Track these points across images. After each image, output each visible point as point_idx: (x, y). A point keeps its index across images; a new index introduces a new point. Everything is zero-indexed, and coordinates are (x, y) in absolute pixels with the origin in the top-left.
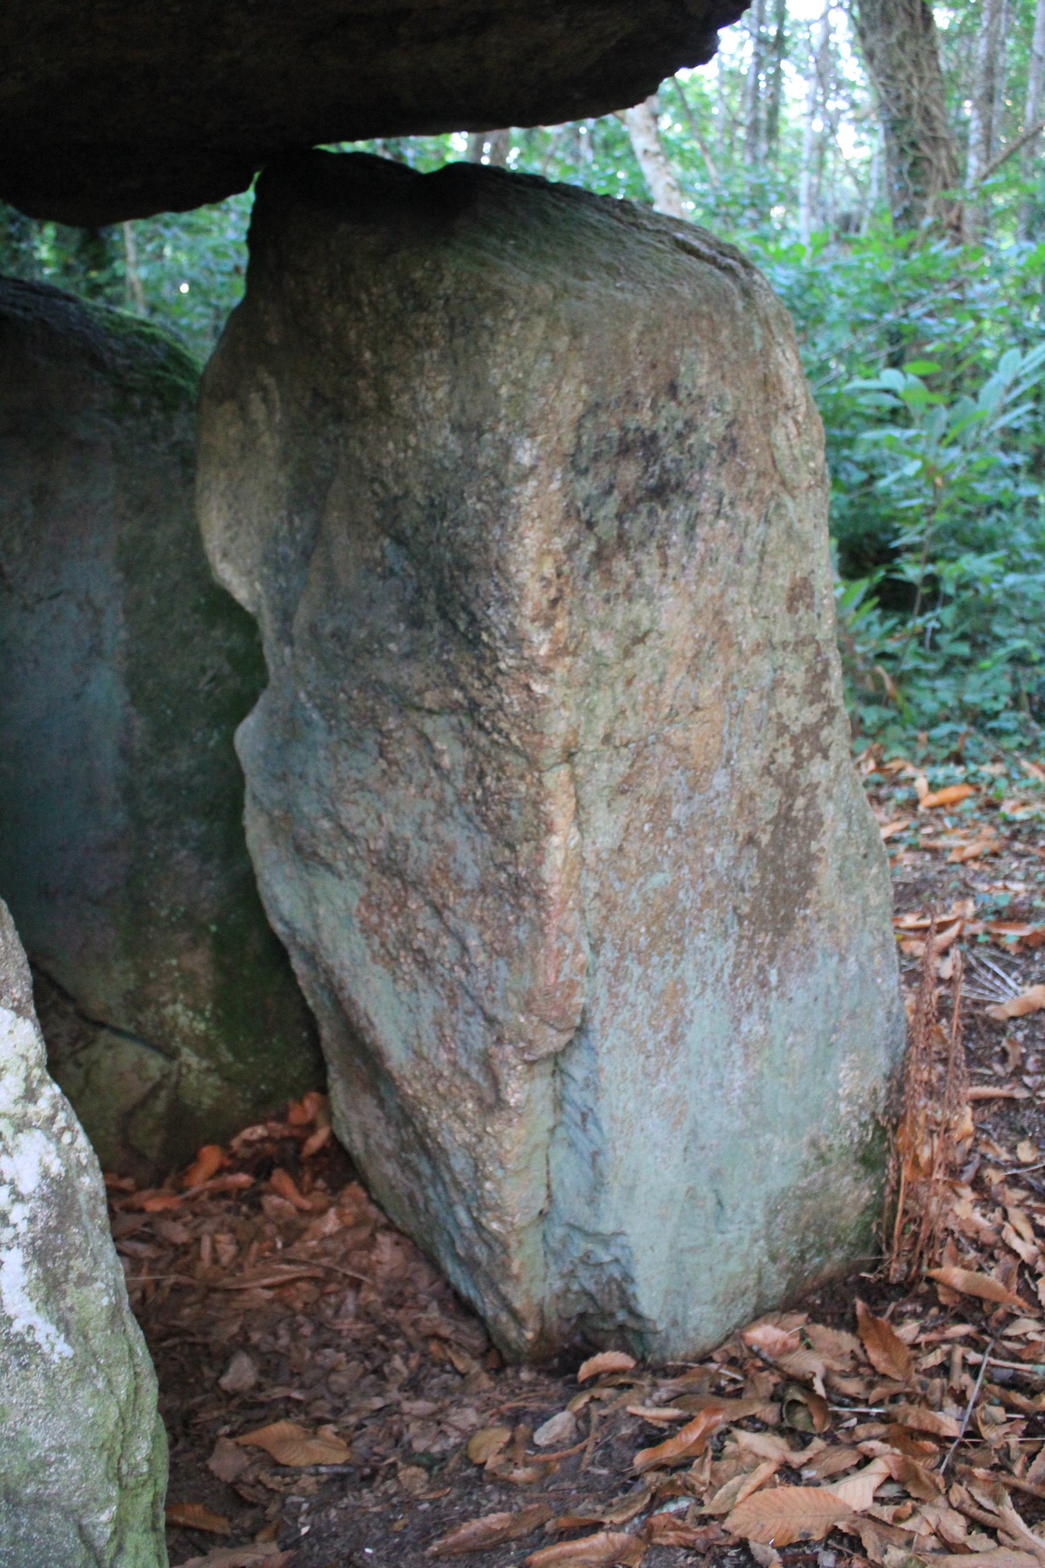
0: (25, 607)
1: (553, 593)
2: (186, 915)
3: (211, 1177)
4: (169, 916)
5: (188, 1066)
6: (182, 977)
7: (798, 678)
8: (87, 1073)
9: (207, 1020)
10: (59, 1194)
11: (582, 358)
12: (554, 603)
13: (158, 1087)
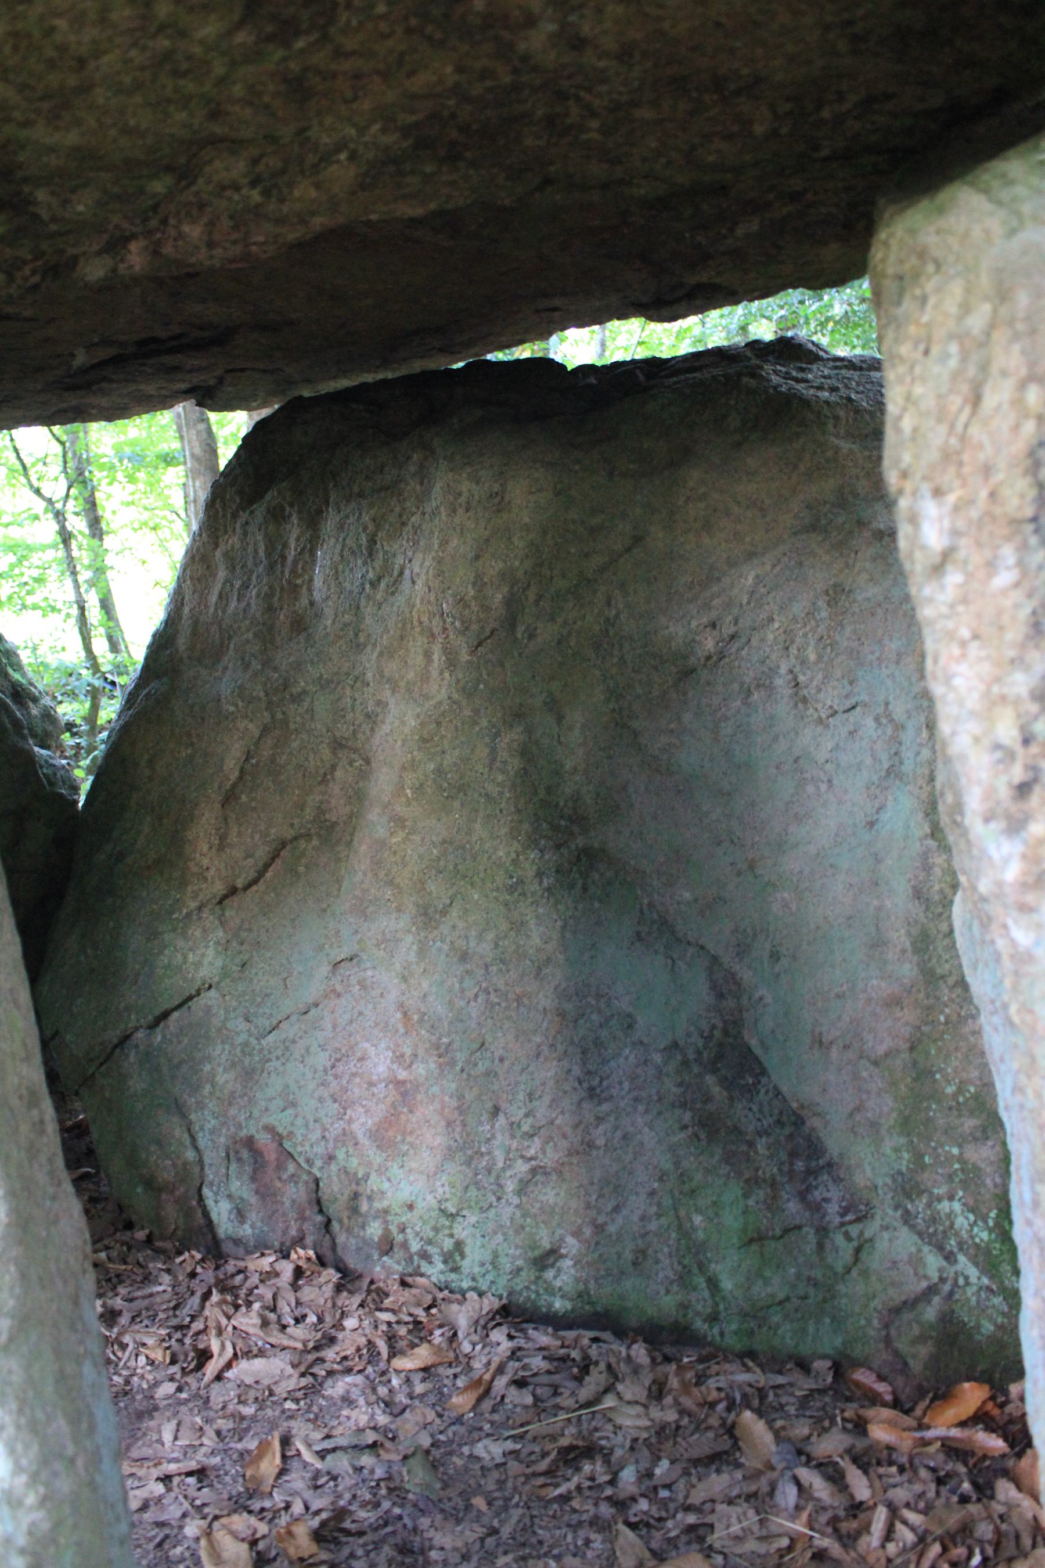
0: (820, 721)
1: (1018, 773)
2: (976, 1097)
3: (962, 1424)
4: (955, 1096)
5: (967, 1278)
6: (962, 1170)
8: (858, 1250)
9: (990, 1230)
11: (1016, 337)
12: (1023, 790)
13: (932, 1290)
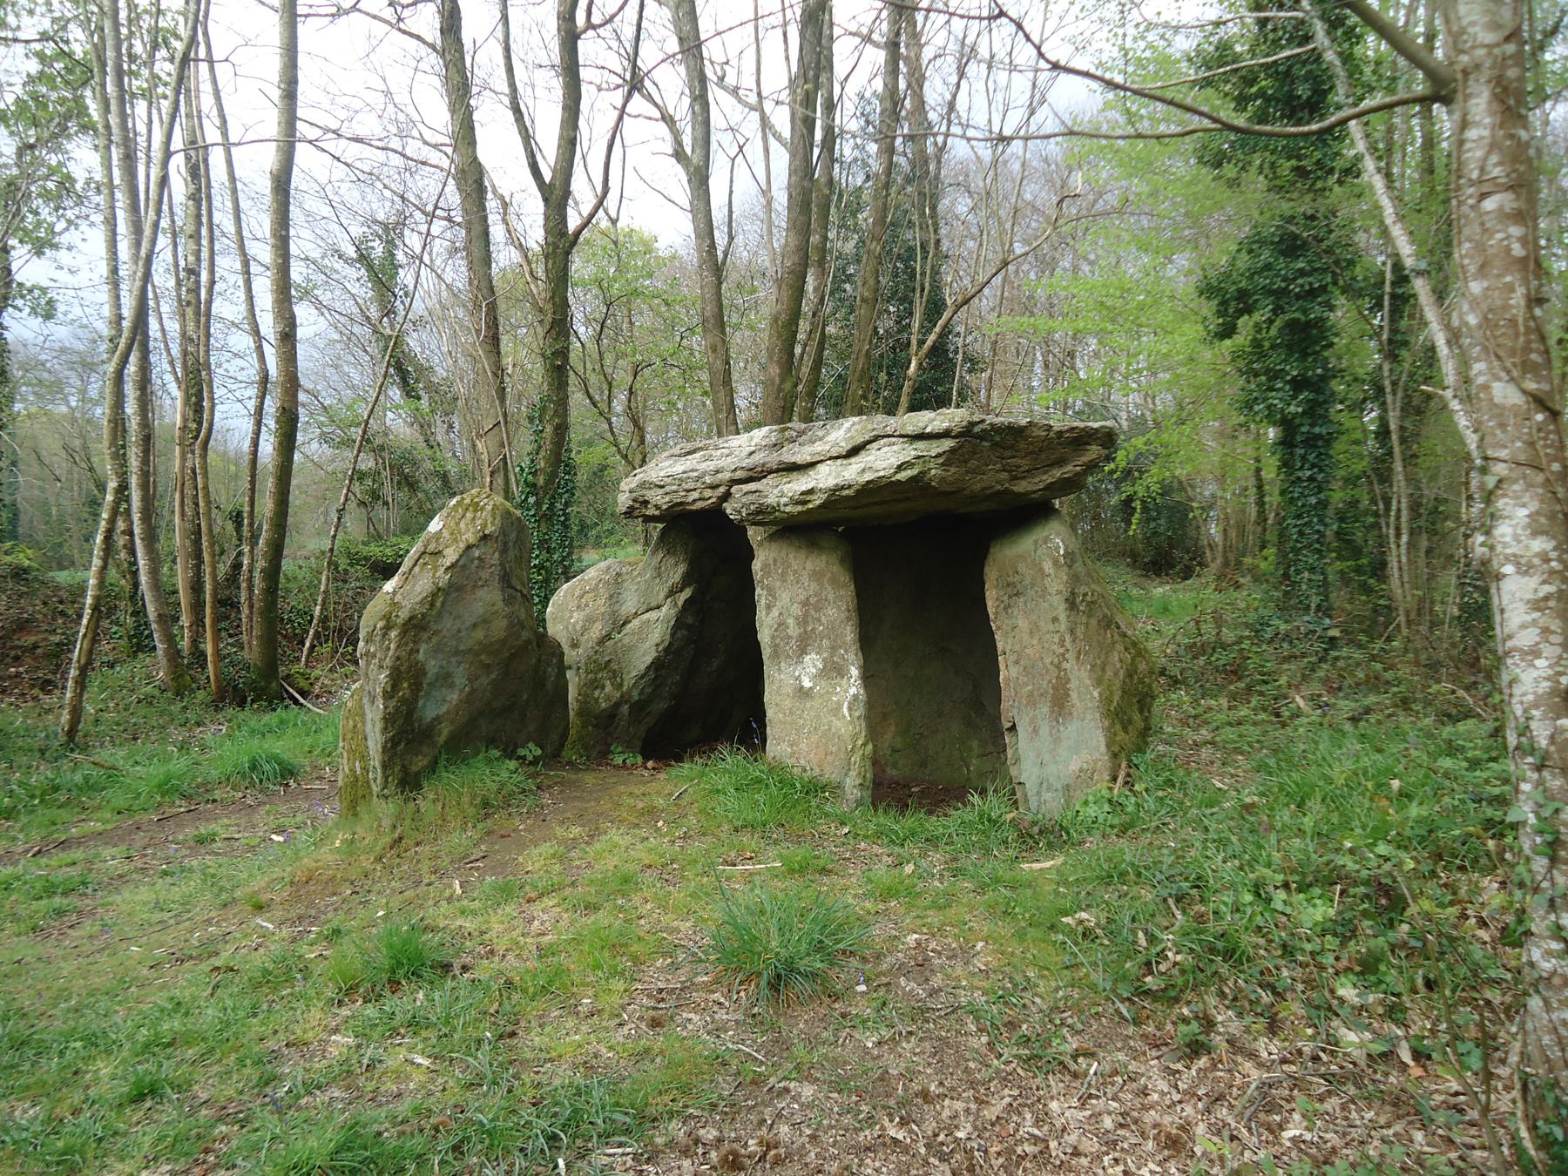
7: (1056, 640)
10: (855, 697)
